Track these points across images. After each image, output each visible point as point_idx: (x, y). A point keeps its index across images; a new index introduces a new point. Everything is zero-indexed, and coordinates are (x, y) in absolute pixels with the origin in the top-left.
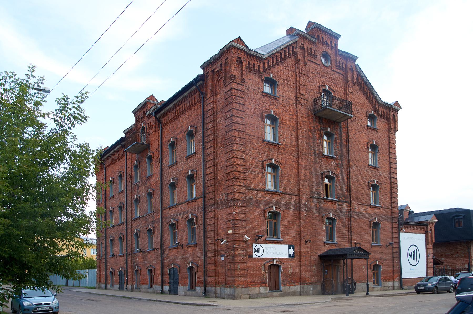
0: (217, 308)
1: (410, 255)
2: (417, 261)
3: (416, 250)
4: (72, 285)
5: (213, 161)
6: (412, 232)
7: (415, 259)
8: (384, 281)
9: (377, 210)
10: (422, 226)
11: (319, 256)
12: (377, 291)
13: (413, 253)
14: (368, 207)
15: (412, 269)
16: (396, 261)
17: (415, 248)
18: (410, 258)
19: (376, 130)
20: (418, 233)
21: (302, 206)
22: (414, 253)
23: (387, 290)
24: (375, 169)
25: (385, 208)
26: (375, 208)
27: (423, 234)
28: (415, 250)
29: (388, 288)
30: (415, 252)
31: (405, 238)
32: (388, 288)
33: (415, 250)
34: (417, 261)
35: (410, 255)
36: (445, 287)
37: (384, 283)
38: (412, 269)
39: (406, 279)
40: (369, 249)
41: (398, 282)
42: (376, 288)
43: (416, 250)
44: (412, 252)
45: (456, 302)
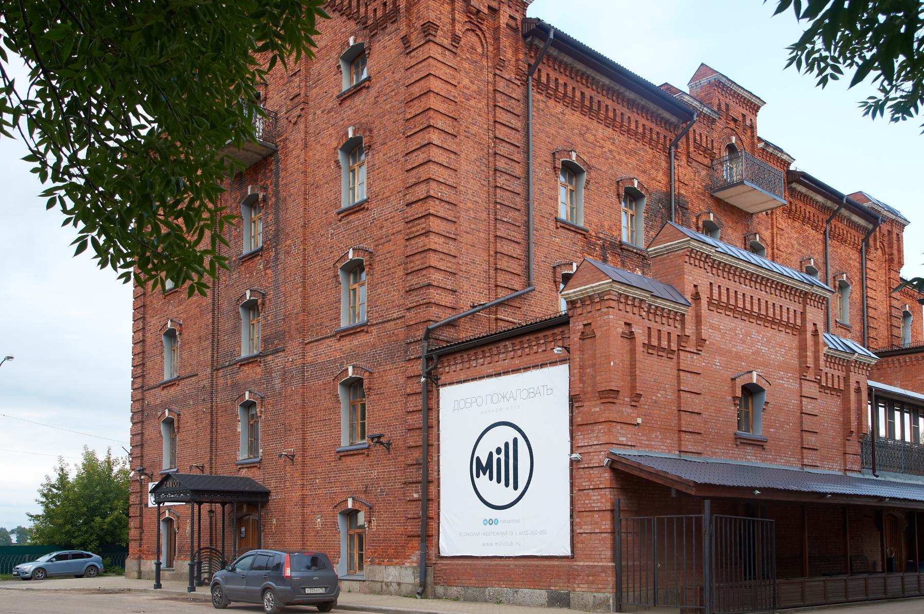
0: (8, 586)
1: (481, 468)
2: (516, 488)
3: (515, 441)
5: (141, 344)
6: (462, 378)
7: (509, 477)
8: (372, 562)
9: (361, 339)
10: (556, 331)
11: (267, 494)
12: (349, 592)
13: (495, 456)
14: (331, 342)
15: (491, 522)
16: (416, 496)
17: (509, 434)
18: (483, 481)
19: (361, 89)
20: (526, 369)
21: (770, 227)
22: (502, 456)
23: (380, 593)
24: (357, 211)
25: (383, 322)
26: (350, 334)
27: (553, 363)
28: (507, 445)
29: (384, 587)
30: (510, 451)
31: (462, 403)
32: (384, 587)
33: (507, 445)
34: (516, 488)
35: (481, 468)
36: (243, 587)
37: (371, 567)
38: (491, 522)
39: (547, 563)
40: (333, 464)
41: (414, 568)
42: (346, 582)
43: (515, 441)
44: (491, 454)
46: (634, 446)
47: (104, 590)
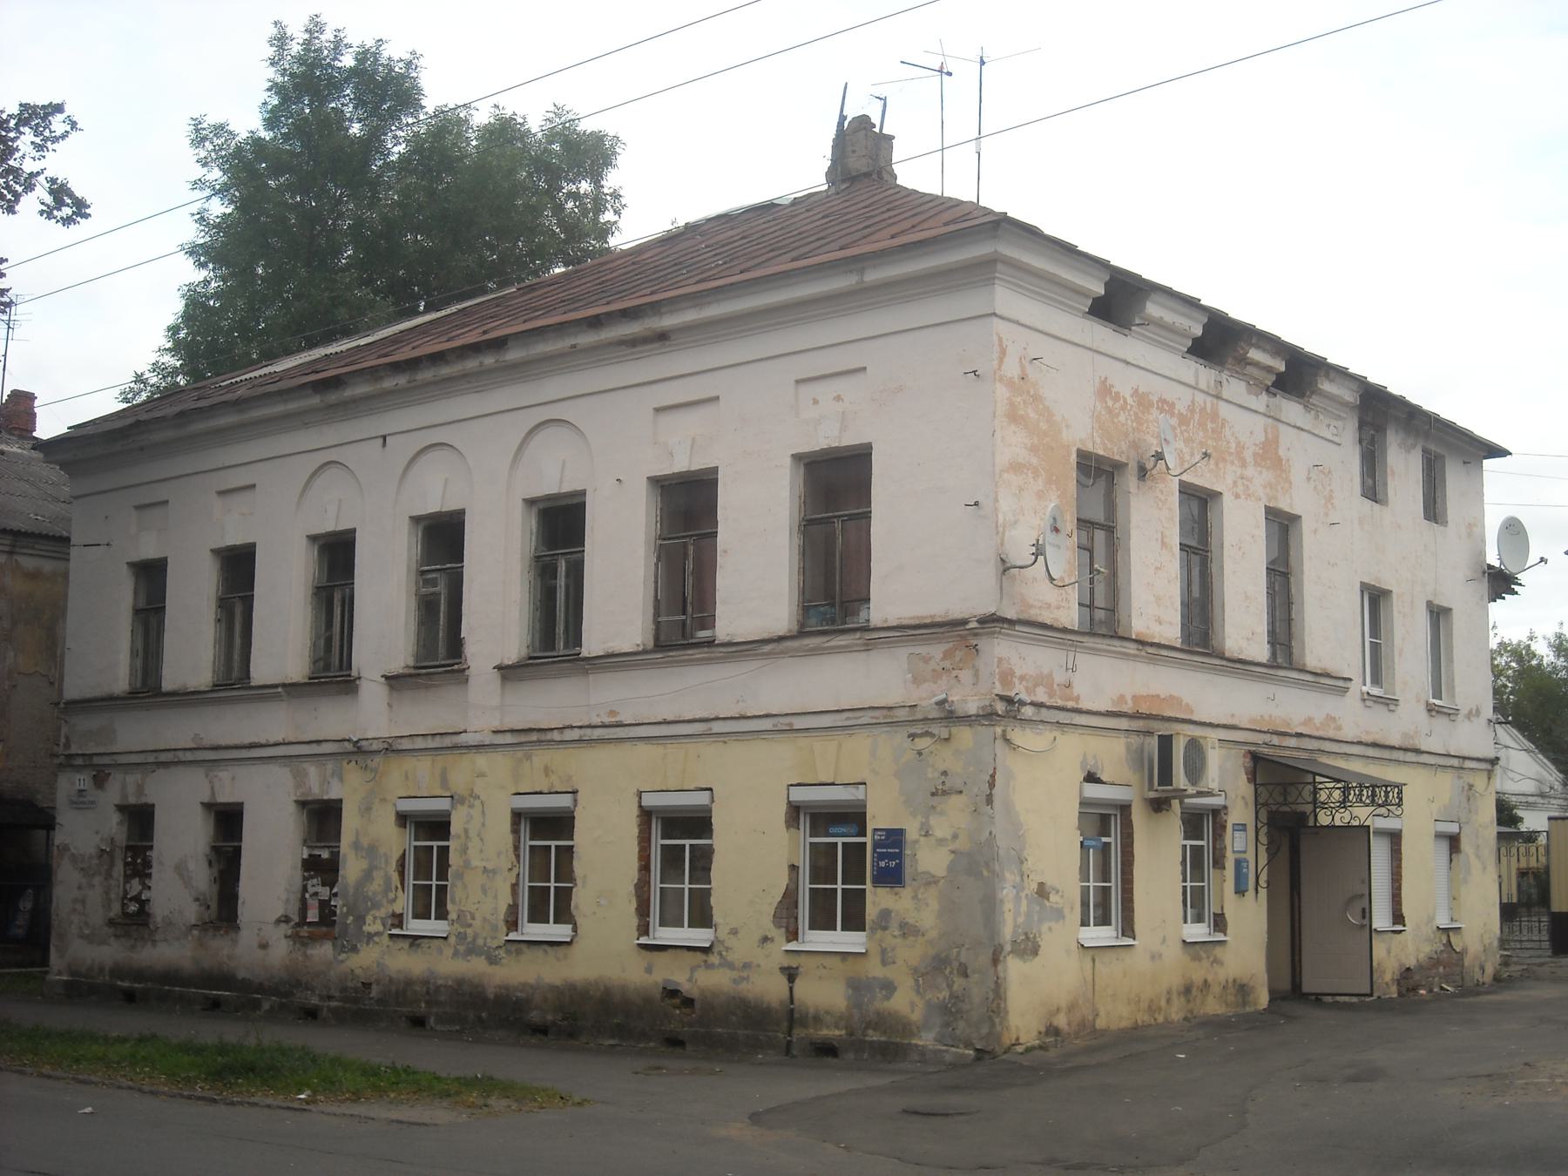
4: (1235, 849)
45: (63, 208)
46: (400, 798)
47: (641, 858)
